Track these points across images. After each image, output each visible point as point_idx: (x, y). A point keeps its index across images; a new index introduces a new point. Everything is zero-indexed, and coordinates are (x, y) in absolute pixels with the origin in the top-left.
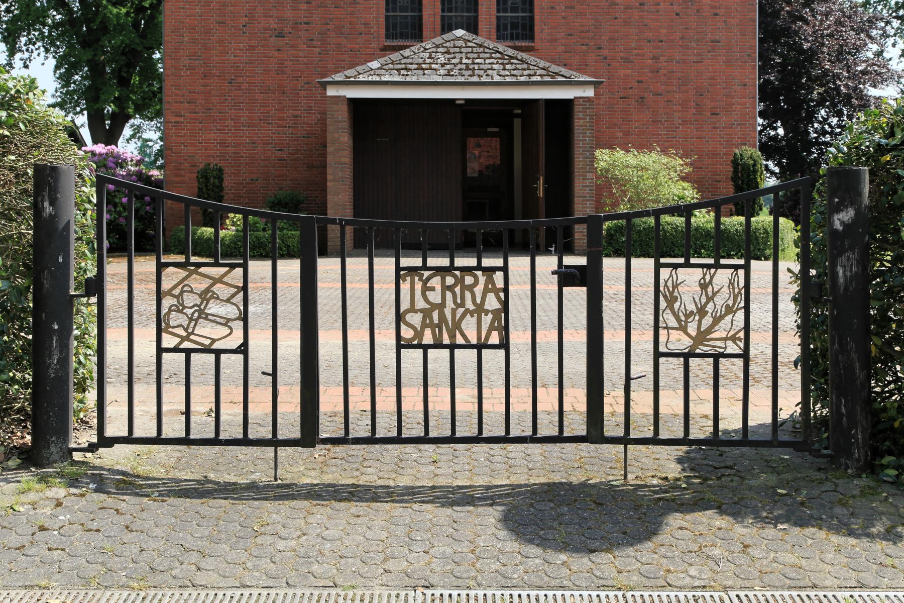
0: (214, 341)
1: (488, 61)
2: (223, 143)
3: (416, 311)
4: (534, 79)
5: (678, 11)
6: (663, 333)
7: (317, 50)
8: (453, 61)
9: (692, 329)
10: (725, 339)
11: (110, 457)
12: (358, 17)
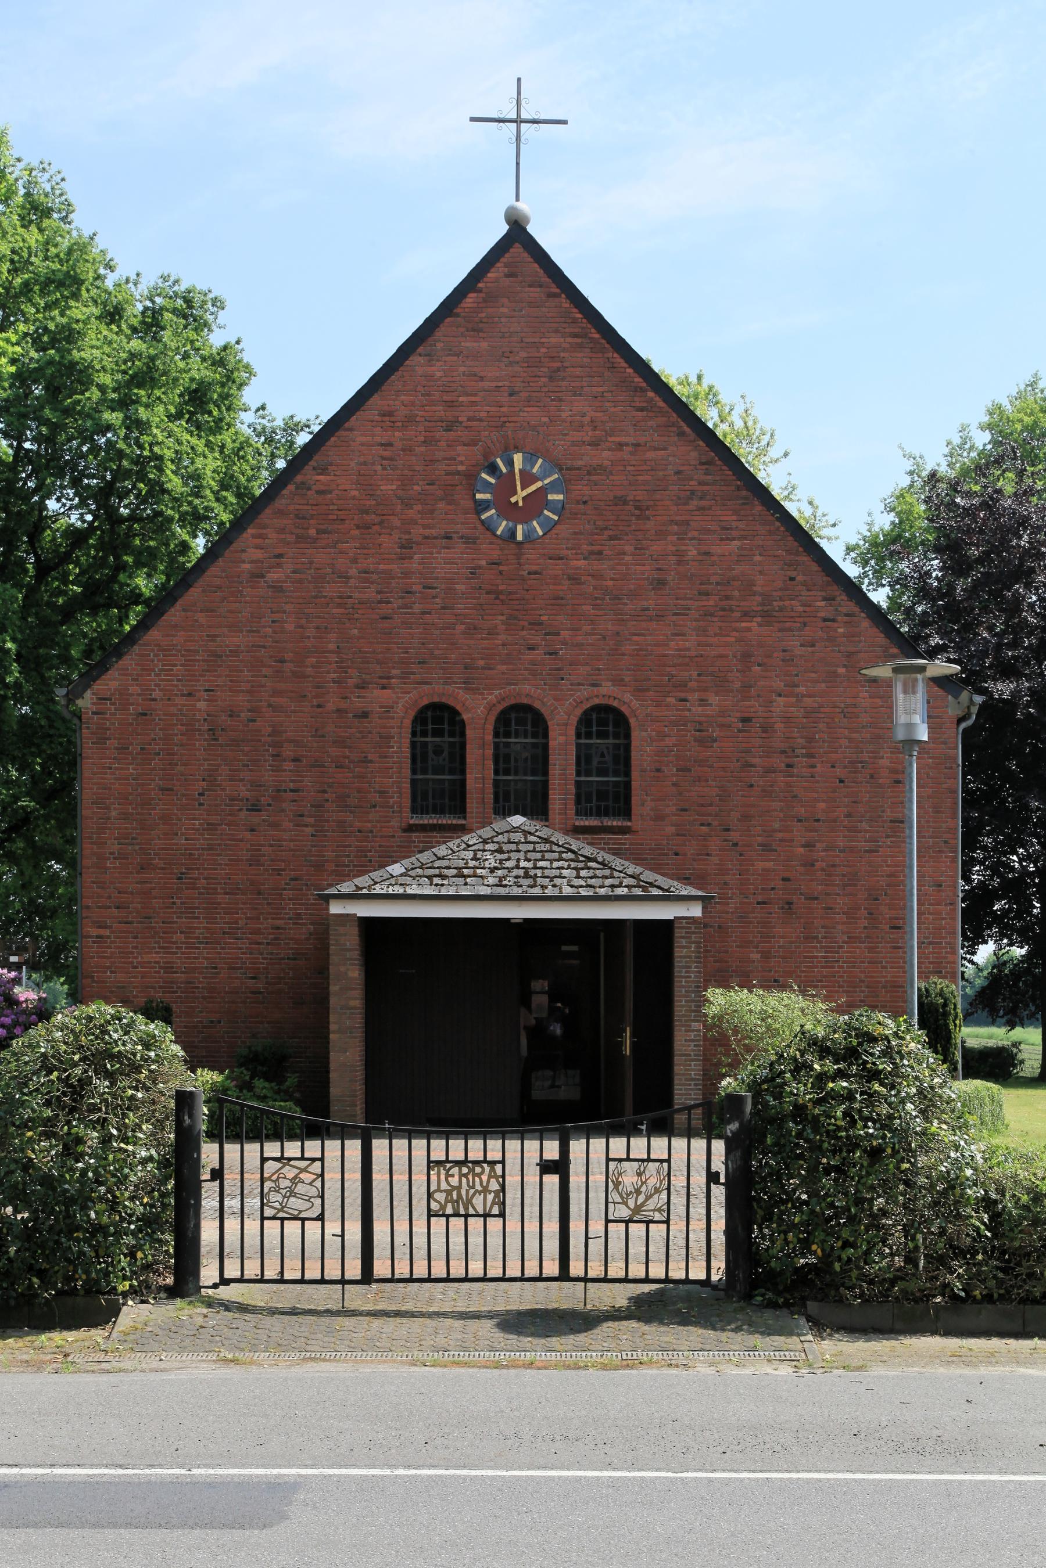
0: (300, 1212)
1: (556, 864)
2: (169, 968)
3: (441, 1191)
4: (619, 891)
5: (843, 777)
6: (611, 1206)
7: (309, 830)
8: (508, 864)
9: (631, 1203)
10: (654, 1211)
11: (224, 1293)
12: (370, 782)
